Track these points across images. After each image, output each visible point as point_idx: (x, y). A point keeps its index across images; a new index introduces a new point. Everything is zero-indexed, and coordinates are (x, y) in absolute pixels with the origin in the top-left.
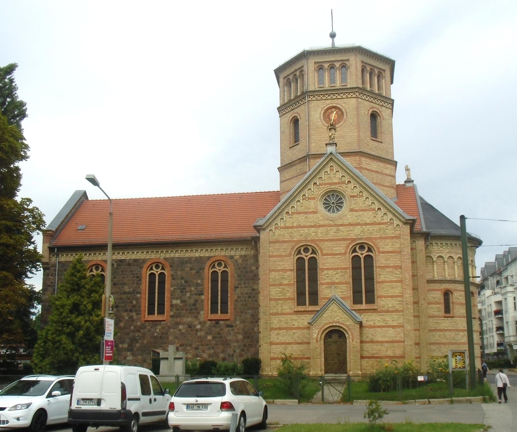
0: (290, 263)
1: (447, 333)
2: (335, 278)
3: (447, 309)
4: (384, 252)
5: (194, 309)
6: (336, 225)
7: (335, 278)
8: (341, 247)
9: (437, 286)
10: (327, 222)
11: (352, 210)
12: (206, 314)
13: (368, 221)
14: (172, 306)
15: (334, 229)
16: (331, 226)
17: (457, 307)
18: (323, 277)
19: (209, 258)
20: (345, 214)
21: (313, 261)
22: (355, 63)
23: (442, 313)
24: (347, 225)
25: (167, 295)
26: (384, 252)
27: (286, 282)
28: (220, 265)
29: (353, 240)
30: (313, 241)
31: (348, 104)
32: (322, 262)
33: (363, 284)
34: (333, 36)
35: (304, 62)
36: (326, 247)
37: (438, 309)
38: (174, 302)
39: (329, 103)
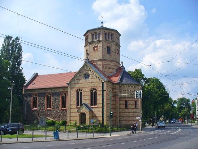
0: (89, 94)
1: (125, 114)
2: (86, 99)
3: (136, 107)
4: (99, 90)
5: (58, 107)
6: (87, 83)
7: (86, 99)
8: (89, 89)
9: (123, 99)
10: (85, 82)
11: (91, 78)
12: (60, 108)
13: (96, 81)
14: (52, 105)
15: (87, 84)
16: (85, 83)
17: (130, 105)
18: (83, 98)
19: (61, 92)
20: (90, 79)
21: (81, 93)
22: (102, 32)
23: (124, 107)
24: (90, 83)
25: (51, 102)
26: (99, 90)
27: (74, 99)
28: (64, 94)
29: (92, 87)
30: (81, 87)
31: (100, 45)
32: (84, 93)
33: (93, 100)
34: (102, 23)
35: (101, 30)
36: (84, 89)
37: (123, 106)
38: (53, 104)
39: (94, 45)
